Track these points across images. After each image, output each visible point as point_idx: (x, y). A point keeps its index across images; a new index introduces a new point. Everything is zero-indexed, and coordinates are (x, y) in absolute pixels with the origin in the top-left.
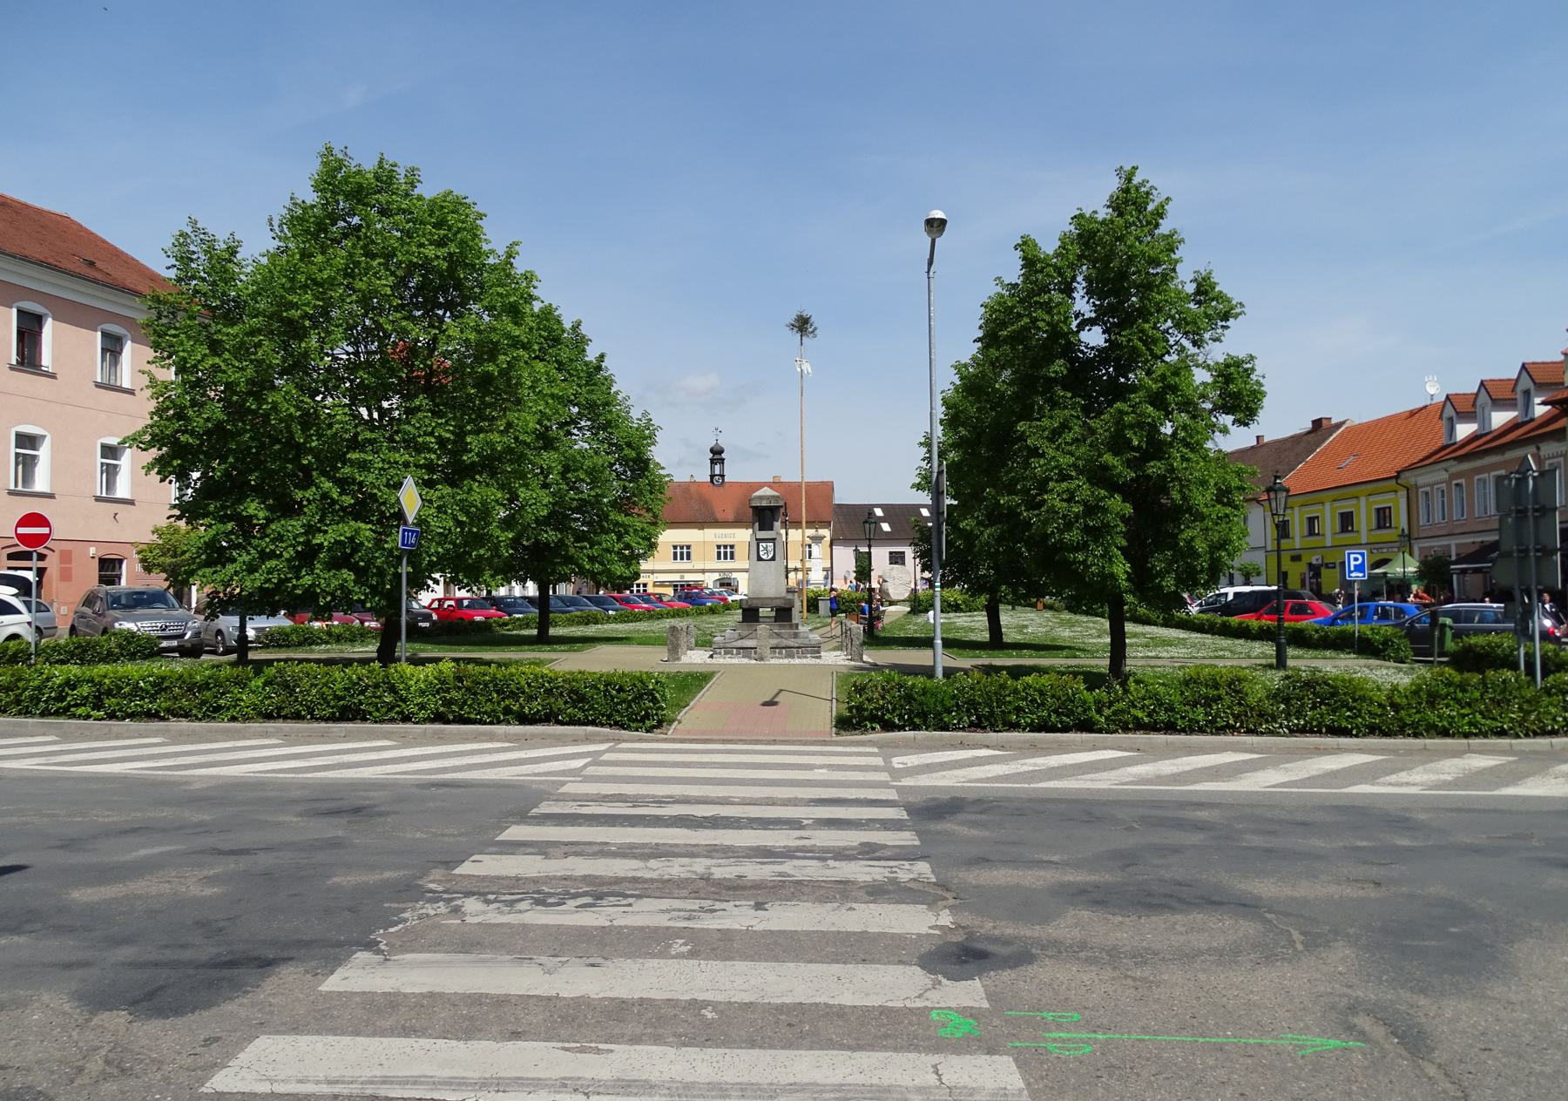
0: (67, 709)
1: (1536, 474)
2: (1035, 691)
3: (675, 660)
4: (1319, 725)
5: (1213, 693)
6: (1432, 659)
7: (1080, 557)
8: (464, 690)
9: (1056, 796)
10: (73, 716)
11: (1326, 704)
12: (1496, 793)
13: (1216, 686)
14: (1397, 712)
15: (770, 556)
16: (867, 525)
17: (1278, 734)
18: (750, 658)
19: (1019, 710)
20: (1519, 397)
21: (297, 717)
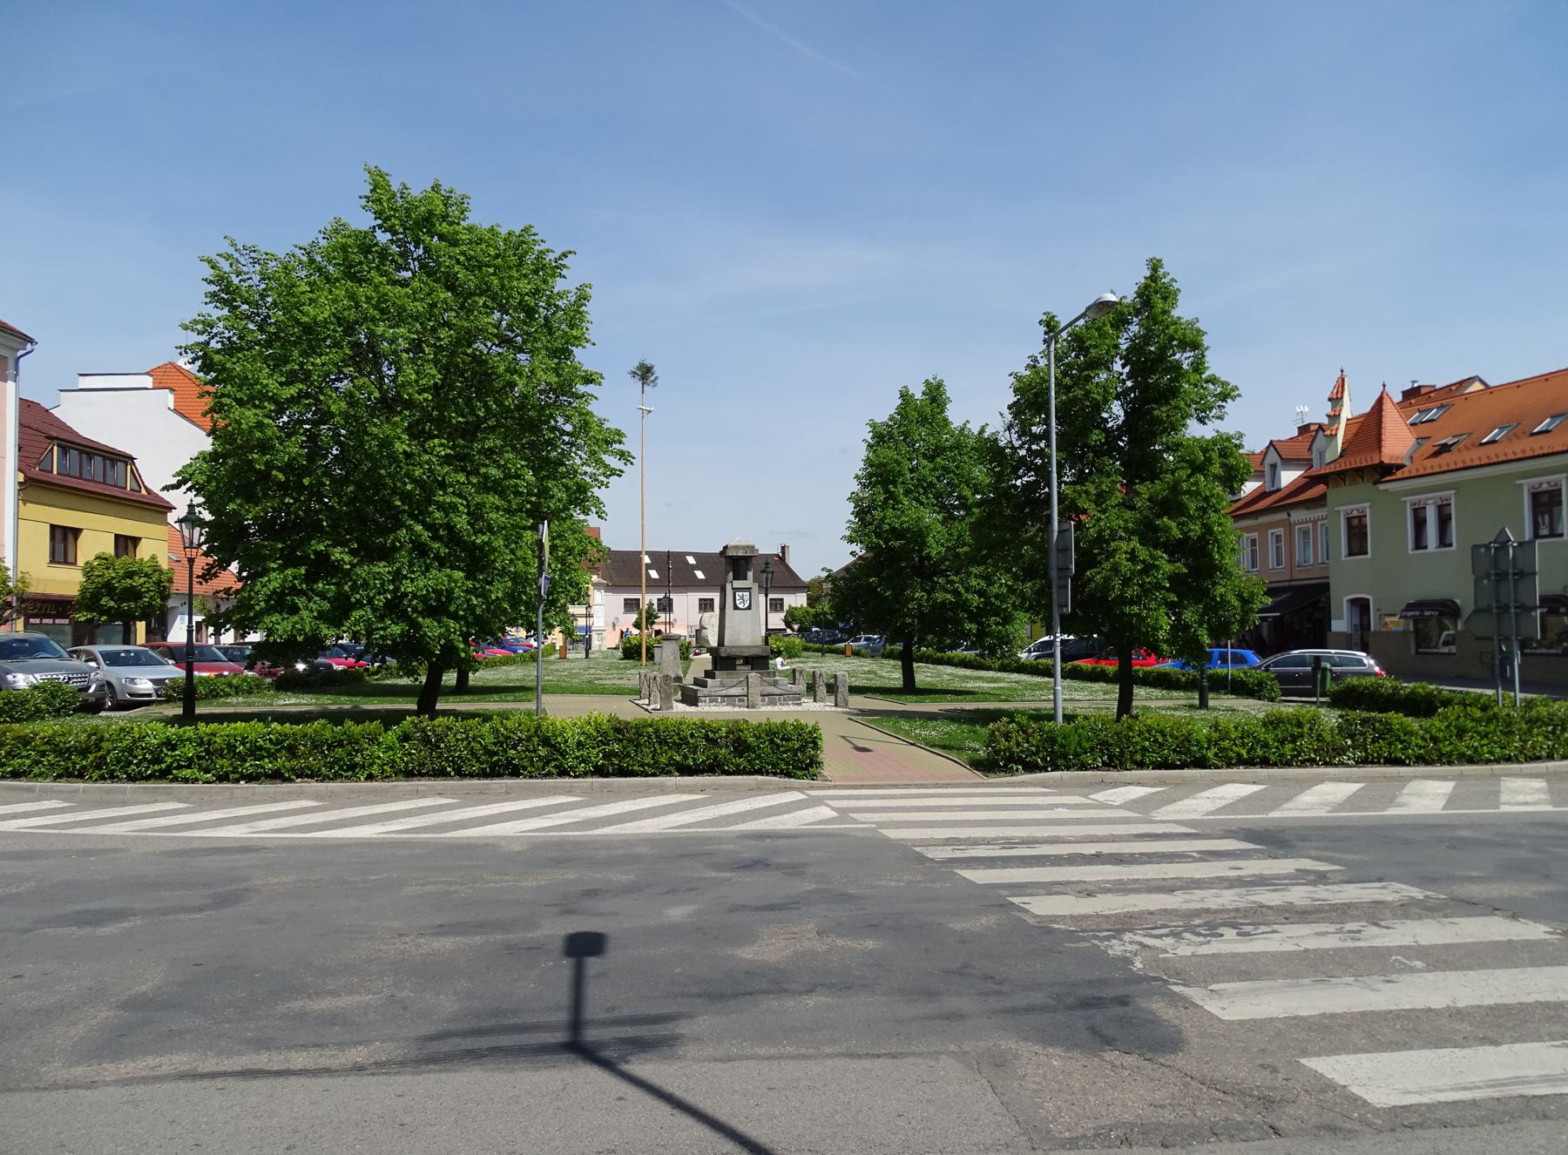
0: (168, 771)
1: (1515, 544)
2: (1157, 732)
3: (668, 709)
4: (1380, 756)
5: (1296, 730)
6: (1314, 699)
7: (1136, 609)
8: (625, 742)
9: (1446, 822)
10: (175, 780)
11: (1384, 739)
12: (590, 833)
13: (1299, 725)
14: (1435, 743)
15: (747, 605)
16: (765, 575)
17: (1347, 765)
18: (734, 706)
19: (1144, 749)
20: (1267, 469)
21: (441, 773)
